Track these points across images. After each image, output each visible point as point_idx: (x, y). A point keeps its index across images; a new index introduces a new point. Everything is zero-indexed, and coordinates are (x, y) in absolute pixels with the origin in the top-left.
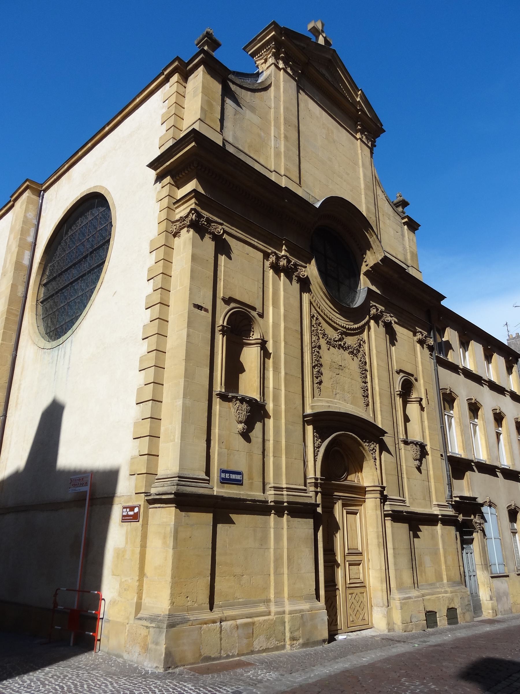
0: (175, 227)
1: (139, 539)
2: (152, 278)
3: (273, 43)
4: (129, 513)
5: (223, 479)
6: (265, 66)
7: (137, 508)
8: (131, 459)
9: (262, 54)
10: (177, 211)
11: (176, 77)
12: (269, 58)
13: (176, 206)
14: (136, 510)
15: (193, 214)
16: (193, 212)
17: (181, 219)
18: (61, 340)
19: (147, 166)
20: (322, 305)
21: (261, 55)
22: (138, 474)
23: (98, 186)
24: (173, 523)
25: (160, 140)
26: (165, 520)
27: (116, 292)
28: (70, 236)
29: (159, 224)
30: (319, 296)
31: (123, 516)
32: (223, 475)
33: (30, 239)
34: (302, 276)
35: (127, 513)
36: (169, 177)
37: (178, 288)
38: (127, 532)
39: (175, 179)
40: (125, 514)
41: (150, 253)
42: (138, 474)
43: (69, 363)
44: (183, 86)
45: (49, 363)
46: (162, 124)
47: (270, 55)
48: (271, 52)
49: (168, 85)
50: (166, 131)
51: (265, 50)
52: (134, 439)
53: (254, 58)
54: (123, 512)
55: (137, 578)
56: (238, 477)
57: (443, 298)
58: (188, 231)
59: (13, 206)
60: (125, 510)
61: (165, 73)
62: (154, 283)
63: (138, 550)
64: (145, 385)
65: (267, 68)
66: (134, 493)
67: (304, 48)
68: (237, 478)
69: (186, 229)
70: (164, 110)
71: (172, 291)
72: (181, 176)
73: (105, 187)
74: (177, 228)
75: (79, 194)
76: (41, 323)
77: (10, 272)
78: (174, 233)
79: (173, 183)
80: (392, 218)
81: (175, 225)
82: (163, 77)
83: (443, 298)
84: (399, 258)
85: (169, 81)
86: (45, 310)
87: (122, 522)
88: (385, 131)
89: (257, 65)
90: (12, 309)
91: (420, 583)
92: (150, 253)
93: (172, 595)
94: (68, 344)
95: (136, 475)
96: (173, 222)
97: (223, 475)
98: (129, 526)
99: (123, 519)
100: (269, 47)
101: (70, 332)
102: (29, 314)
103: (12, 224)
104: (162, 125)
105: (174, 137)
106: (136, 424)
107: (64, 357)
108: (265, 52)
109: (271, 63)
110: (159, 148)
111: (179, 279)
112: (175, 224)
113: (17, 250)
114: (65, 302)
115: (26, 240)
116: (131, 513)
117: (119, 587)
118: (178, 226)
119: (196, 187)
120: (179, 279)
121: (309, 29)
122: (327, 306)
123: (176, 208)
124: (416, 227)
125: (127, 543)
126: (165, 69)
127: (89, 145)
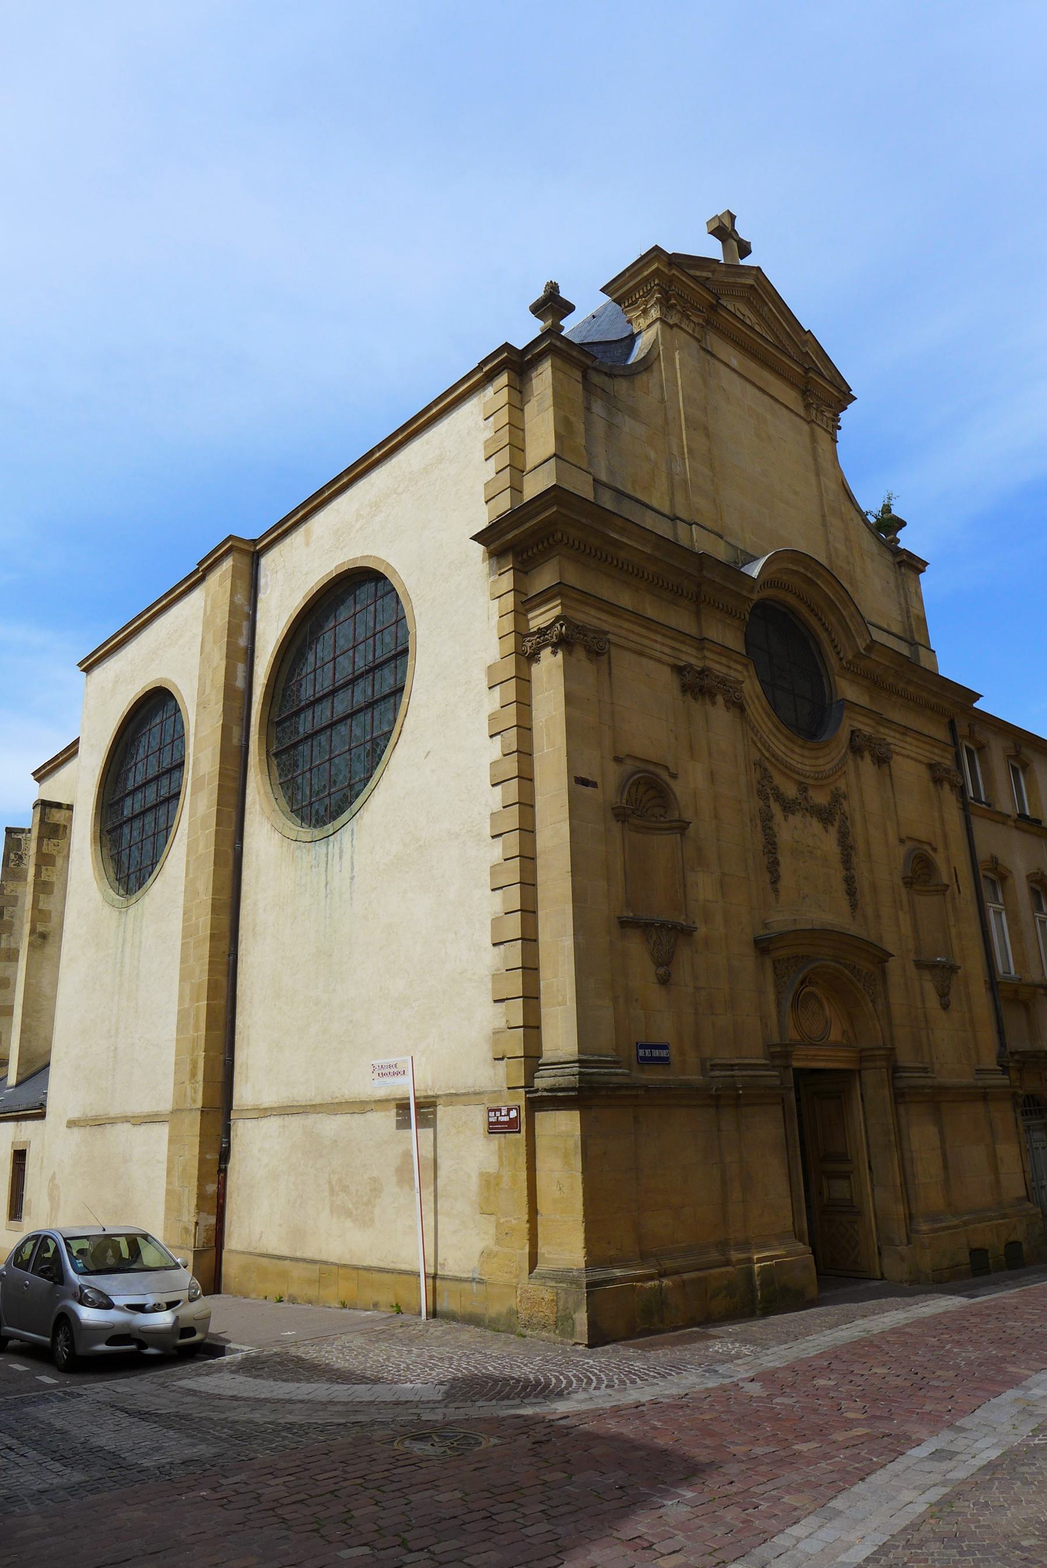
1: (522, 1159)
2: (499, 733)
4: (500, 1118)
5: (644, 1058)
6: (643, 323)
7: (515, 1111)
8: (493, 1033)
11: (503, 379)
15: (561, 625)
18: (330, 828)
20: (774, 747)
22: (509, 1058)
23: (371, 556)
24: (578, 1133)
25: (485, 489)
26: (563, 1128)
27: (429, 752)
29: (500, 638)
31: (490, 1123)
32: (641, 1052)
33: (243, 642)
35: (498, 1118)
37: (546, 751)
38: (500, 1148)
41: (490, 688)
42: (509, 1058)
43: (352, 869)
45: (311, 867)
46: (486, 460)
47: (652, 302)
48: (652, 297)
50: (497, 473)
52: (495, 1001)
54: (489, 1117)
55: (526, 1217)
56: (663, 1053)
57: (977, 696)
58: (554, 653)
60: (492, 1114)
63: (523, 1175)
64: (506, 914)
66: (505, 1086)
67: (708, 279)
68: (662, 1055)
69: (549, 649)
70: (489, 434)
75: (333, 568)
76: (280, 792)
77: (216, 704)
81: (529, 641)
82: (480, 375)
83: (977, 696)
87: (490, 1133)
88: (856, 399)
90: (226, 769)
91: (505, 1137)
93: (587, 1240)
94: (345, 835)
95: (506, 1059)
97: (641, 1052)
98: (503, 1138)
99: (490, 1129)
101: (345, 816)
102: (256, 776)
103: (205, 614)
104: (488, 461)
105: (512, 486)
106: (495, 977)
107: (341, 858)
109: (655, 318)
110: (487, 502)
111: (544, 734)
112: (529, 638)
113: (223, 663)
117: (495, 1230)
119: (561, 576)
120: (544, 734)
124: (920, 566)
125: (501, 1164)
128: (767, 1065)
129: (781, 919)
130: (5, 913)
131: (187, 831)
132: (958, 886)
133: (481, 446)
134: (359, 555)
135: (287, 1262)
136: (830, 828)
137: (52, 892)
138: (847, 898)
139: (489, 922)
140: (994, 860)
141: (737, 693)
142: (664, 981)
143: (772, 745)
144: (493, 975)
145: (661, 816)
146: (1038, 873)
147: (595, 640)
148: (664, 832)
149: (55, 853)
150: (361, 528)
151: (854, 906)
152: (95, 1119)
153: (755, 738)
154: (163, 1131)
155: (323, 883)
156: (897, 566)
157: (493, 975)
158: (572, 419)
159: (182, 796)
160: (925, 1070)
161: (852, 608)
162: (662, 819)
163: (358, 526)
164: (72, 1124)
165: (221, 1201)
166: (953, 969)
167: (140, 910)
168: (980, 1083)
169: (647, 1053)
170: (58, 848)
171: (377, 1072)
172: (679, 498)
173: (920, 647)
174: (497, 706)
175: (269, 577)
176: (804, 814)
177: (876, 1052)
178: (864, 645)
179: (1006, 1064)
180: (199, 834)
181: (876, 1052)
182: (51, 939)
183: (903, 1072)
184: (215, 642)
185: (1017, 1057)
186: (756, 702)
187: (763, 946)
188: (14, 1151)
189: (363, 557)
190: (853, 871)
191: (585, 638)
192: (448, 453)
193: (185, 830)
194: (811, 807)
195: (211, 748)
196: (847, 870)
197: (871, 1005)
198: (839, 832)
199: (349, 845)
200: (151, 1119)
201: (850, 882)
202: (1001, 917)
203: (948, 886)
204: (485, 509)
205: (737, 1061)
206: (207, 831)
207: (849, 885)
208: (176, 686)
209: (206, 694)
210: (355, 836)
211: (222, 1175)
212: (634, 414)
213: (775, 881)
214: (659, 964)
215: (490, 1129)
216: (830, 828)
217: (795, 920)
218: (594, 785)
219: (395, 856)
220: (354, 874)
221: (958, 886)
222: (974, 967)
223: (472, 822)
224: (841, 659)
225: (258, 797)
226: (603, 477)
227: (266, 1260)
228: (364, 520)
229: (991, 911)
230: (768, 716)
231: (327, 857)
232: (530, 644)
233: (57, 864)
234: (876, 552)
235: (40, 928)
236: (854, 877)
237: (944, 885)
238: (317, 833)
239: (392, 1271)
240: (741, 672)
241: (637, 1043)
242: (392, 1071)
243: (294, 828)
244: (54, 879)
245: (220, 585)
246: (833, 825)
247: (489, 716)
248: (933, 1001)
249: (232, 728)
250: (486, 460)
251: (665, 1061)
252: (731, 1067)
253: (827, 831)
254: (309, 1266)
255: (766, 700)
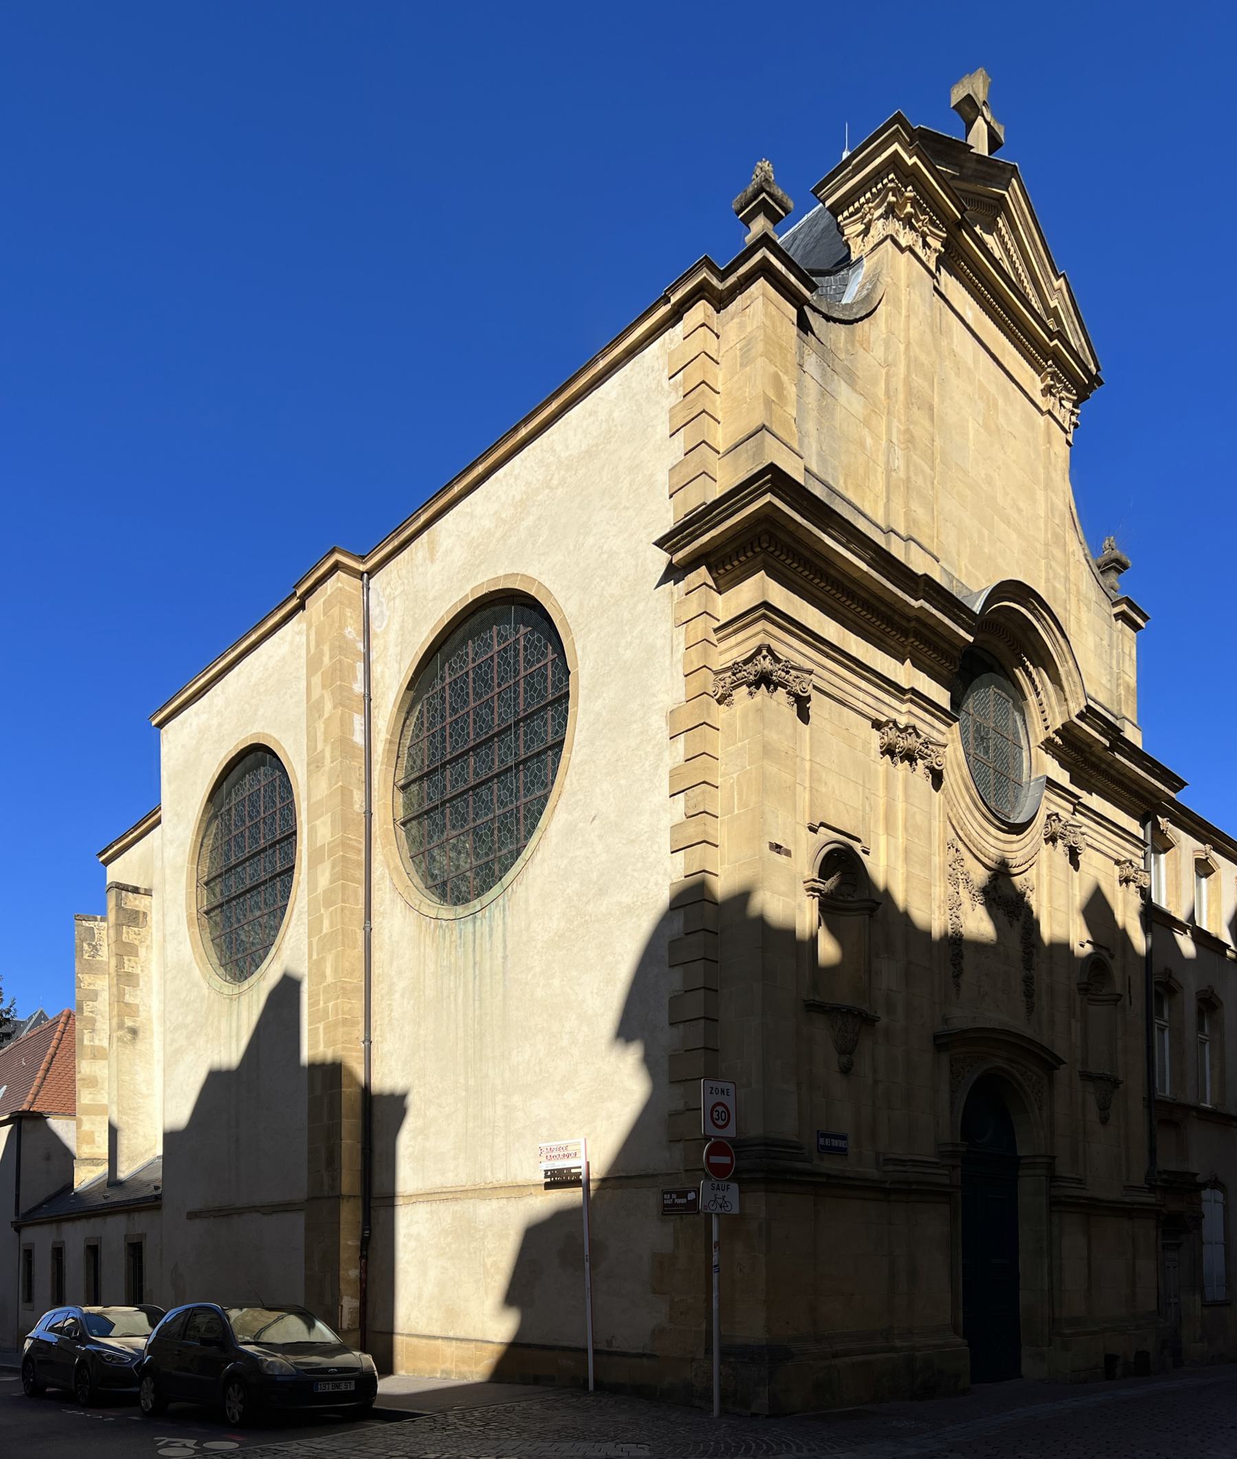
0: (722, 683)
3: (892, 176)
4: (676, 1200)
5: (824, 1147)
8: (670, 1115)
9: (862, 206)
10: (723, 646)
12: (878, 219)
13: (720, 635)
14: (691, 1196)
16: (764, 652)
17: (736, 666)
18: (476, 904)
19: (655, 544)
21: (857, 211)
25: (670, 478)
28: (450, 683)
30: (963, 805)
32: (822, 1141)
34: (937, 767)
36: (703, 569)
37: (736, 812)
39: (715, 575)
40: (669, 1202)
44: (713, 332)
46: (671, 436)
48: (883, 201)
49: (680, 329)
51: (868, 195)
53: (840, 218)
56: (841, 1144)
59: (301, 606)
61: (674, 299)
62: (686, 801)
65: (872, 250)
71: (722, 816)
72: (729, 567)
73: (535, 580)
74: (727, 685)
78: (720, 697)
79: (711, 583)
80: (1093, 606)
84: (1100, 700)
85: (680, 319)
86: (412, 840)
89: (845, 238)
92: (671, 738)
96: (717, 673)
100: (880, 186)
107: (491, 936)
108: (868, 202)
114: (462, 826)
115: (351, 689)
116: (683, 1201)
118: (728, 681)
121: (953, 103)
122: (975, 825)
123: (720, 640)
126: (673, 289)
127: (480, 469)
128: (937, 1163)
129: (962, 1018)
130: (85, 1007)
131: (306, 909)
132: (1130, 997)
133: (665, 417)
134: (501, 573)
135: (440, 1342)
136: (1015, 923)
137: (138, 985)
138: (1024, 999)
139: (666, 1001)
140: (1168, 973)
141: (939, 759)
142: (846, 1070)
143: (967, 823)
144: (670, 1056)
145: (848, 895)
146: (1206, 991)
147: (797, 680)
148: (853, 913)
149: (137, 942)
150: (503, 537)
151: (1030, 1009)
152: (220, 1210)
153: (951, 815)
154: (300, 1219)
155: (471, 964)
156: (1113, 618)
157: (670, 1056)
158: (785, 378)
159: (296, 870)
160: (1080, 1181)
161: (1071, 663)
162: (850, 899)
163: (498, 535)
164: (192, 1215)
165: (364, 1286)
166: (1116, 1083)
167: (255, 997)
168: (1127, 1199)
169: (827, 1143)
170: (139, 937)
171: (544, 1155)
172: (898, 506)
173: (1126, 721)
174: (680, 759)
175: (385, 606)
176: (991, 904)
177: (1038, 1160)
178: (1077, 712)
179: (1153, 1183)
180: (322, 912)
181: (1038, 1160)
182: (141, 1034)
183: (1060, 1181)
184: (324, 687)
185: (1165, 1176)
186: (957, 771)
187: (942, 1042)
188: (129, 1244)
189: (506, 576)
190: (1032, 972)
191: (787, 676)
192: (620, 428)
193: (303, 908)
194: (999, 897)
195: (329, 814)
196: (1028, 969)
197: (1037, 1111)
198: (1024, 928)
199: (500, 923)
200: (285, 1208)
201: (1028, 981)
202: (1163, 1034)
203: (1120, 996)
204: (669, 504)
205: (911, 1157)
206: (331, 909)
207: (1027, 986)
208: (277, 742)
209: (318, 751)
210: (507, 913)
211: (363, 1261)
212: (851, 378)
213: (957, 976)
214: (842, 1052)
215: (665, 1211)
216: (1015, 923)
217: (975, 1018)
218: (788, 853)
219: (556, 933)
220: (507, 953)
221: (1130, 997)
222: (1135, 1084)
223: (648, 894)
224: (1047, 728)
225: (387, 871)
226: (814, 468)
227: (414, 1341)
228: (507, 527)
229: (1156, 1025)
230: (967, 789)
231: (475, 936)
232: (722, 683)
233: (140, 954)
234: (1094, 599)
235: (129, 1023)
236: (1033, 977)
237: (1118, 995)
238: (460, 910)
239: (551, 1348)
240: (943, 734)
241: (818, 1132)
242: (562, 1153)
243: (431, 906)
244: (138, 971)
245: (325, 614)
246: (1018, 920)
247: (670, 771)
248: (1093, 1115)
249: (352, 791)
250: (671, 436)
251: (843, 1151)
252: (902, 1162)
253: (1011, 926)
254: (463, 1345)
255: (967, 770)
